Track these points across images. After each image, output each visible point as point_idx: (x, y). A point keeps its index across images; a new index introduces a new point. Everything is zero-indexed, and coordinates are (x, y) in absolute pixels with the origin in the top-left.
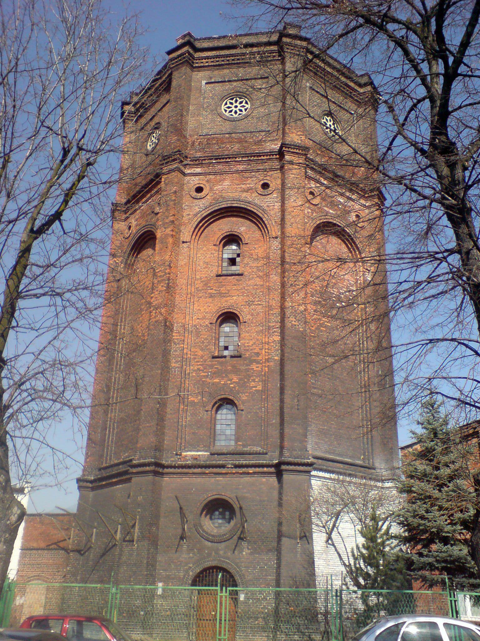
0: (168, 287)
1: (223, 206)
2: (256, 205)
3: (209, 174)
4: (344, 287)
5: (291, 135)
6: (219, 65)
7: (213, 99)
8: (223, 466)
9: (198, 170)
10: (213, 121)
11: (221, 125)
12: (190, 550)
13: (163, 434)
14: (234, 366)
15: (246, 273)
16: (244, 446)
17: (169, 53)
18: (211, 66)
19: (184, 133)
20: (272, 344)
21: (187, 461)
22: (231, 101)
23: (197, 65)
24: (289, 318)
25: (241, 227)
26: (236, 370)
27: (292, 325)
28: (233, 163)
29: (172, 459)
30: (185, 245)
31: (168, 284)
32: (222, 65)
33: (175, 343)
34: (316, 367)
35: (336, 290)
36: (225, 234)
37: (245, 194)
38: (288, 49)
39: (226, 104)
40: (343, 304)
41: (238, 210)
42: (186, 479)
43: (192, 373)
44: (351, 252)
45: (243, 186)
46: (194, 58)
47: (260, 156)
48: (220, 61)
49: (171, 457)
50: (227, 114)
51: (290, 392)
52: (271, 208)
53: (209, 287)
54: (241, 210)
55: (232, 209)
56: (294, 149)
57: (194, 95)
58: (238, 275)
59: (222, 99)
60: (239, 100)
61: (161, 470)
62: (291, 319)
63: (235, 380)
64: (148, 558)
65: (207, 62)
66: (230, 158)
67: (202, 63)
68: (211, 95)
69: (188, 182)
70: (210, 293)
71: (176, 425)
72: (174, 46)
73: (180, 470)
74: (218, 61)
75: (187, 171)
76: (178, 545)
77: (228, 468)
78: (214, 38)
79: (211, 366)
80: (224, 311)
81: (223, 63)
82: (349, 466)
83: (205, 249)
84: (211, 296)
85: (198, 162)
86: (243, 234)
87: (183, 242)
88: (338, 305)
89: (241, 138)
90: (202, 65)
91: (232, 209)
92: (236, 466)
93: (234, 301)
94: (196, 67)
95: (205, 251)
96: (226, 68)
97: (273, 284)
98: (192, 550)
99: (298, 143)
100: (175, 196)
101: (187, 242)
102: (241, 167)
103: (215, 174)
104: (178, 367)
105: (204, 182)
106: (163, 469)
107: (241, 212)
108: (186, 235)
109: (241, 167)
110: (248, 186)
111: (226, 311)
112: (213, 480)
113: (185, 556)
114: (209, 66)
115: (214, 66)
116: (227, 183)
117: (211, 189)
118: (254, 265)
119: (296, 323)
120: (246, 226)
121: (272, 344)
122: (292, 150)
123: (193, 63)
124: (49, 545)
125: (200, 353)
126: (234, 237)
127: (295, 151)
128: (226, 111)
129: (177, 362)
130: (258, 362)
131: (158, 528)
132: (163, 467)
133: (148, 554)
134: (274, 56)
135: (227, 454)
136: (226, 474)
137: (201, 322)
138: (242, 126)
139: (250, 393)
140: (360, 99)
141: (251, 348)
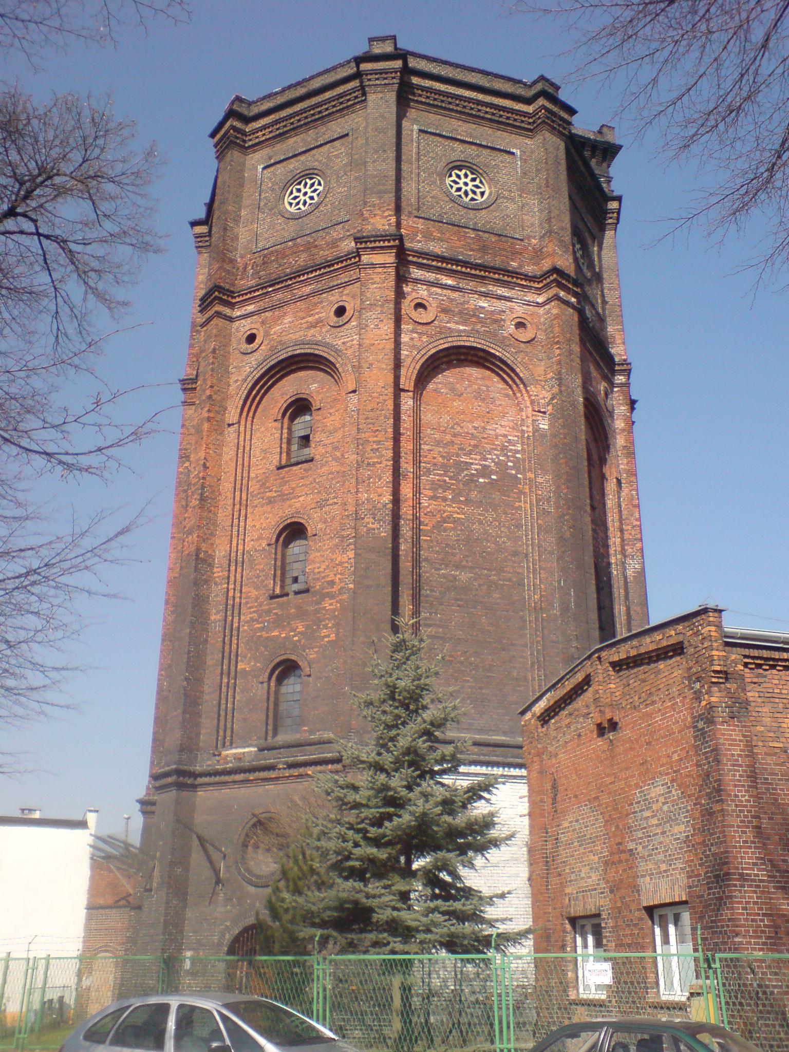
0: (202, 499)
1: (285, 356)
2: (326, 345)
3: (265, 310)
4: (495, 449)
5: (372, 221)
6: (281, 135)
7: (273, 190)
8: (271, 768)
9: (251, 308)
10: (272, 226)
11: (284, 228)
12: (228, 900)
13: (198, 725)
14: (298, 608)
15: (317, 457)
16: (311, 732)
17: (213, 135)
18: (270, 138)
19: (230, 255)
20: (346, 565)
21: (227, 763)
22: (298, 187)
23: (250, 143)
24: (363, 519)
25: (307, 383)
26: (301, 614)
27: (369, 530)
28: (297, 286)
29: (209, 763)
30: (231, 429)
31: (202, 494)
32: (287, 132)
33: (216, 584)
34: (432, 591)
35: (478, 457)
36: (290, 400)
37: (312, 331)
38: (369, 80)
39: (291, 193)
40: (494, 477)
41: (304, 358)
42: (226, 792)
43: (243, 626)
44: (511, 388)
45: (310, 319)
46: (244, 134)
47: (333, 265)
48: (281, 128)
49: (208, 759)
50: (293, 209)
51: (361, 638)
52: (348, 344)
53: (268, 488)
54: (292, 361)
55: (296, 359)
56: (375, 241)
57: (248, 189)
58: (306, 461)
59: (285, 188)
60: (309, 182)
61: (190, 781)
62: (366, 520)
63: (301, 628)
64: (166, 914)
65: (264, 135)
66: (291, 279)
67: (257, 137)
68: (270, 185)
69: (238, 330)
70: (268, 498)
71: (216, 709)
72: (215, 124)
73: (217, 779)
74: (278, 129)
75: (237, 313)
76: (213, 894)
77: (280, 769)
78: (276, 93)
79: (269, 612)
80: (286, 523)
81: (285, 129)
82: (491, 749)
83: (263, 429)
84: (270, 502)
85: (250, 295)
86: (314, 394)
87: (229, 425)
88: (481, 480)
89: (309, 243)
90: (257, 140)
91: (296, 359)
92: (291, 766)
93: (302, 504)
94: (250, 147)
95: (263, 432)
96: (290, 137)
97: (349, 468)
98: (231, 899)
99: (384, 230)
100: (214, 357)
101: (233, 424)
102: (307, 290)
103: (272, 308)
104: (220, 621)
105: (257, 326)
106: (195, 779)
107: (308, 361)
108: (232, 415)
109: (307, 290)
110: (317, 316)
111: (289, 521)
112: (260, 790)
113: (221, 909)
114: (267, 140)
115: (274, 137)
116: (288, 319)
117: (267, 334)
118: (329, 442)
119: (374, 526)
120: (319, 382)
121: (346, 565)
122: (373, 245)
123: (245, 141)
124: (117, 901)
125: (254, 593)
126: (303, 403)
127: (377, 244)
128: (291, 204)
129: (218, 612)
130: (331, 596)
131: (187, 870)
132: (195, 775)
133: (167, 909)
134: (356, 97)
135: (280, 748)
136: (277, 778)
137: (256, 545)
138: (310, 223)
139: (321, 646)
140: (529, 123)
141: (323, 575)
